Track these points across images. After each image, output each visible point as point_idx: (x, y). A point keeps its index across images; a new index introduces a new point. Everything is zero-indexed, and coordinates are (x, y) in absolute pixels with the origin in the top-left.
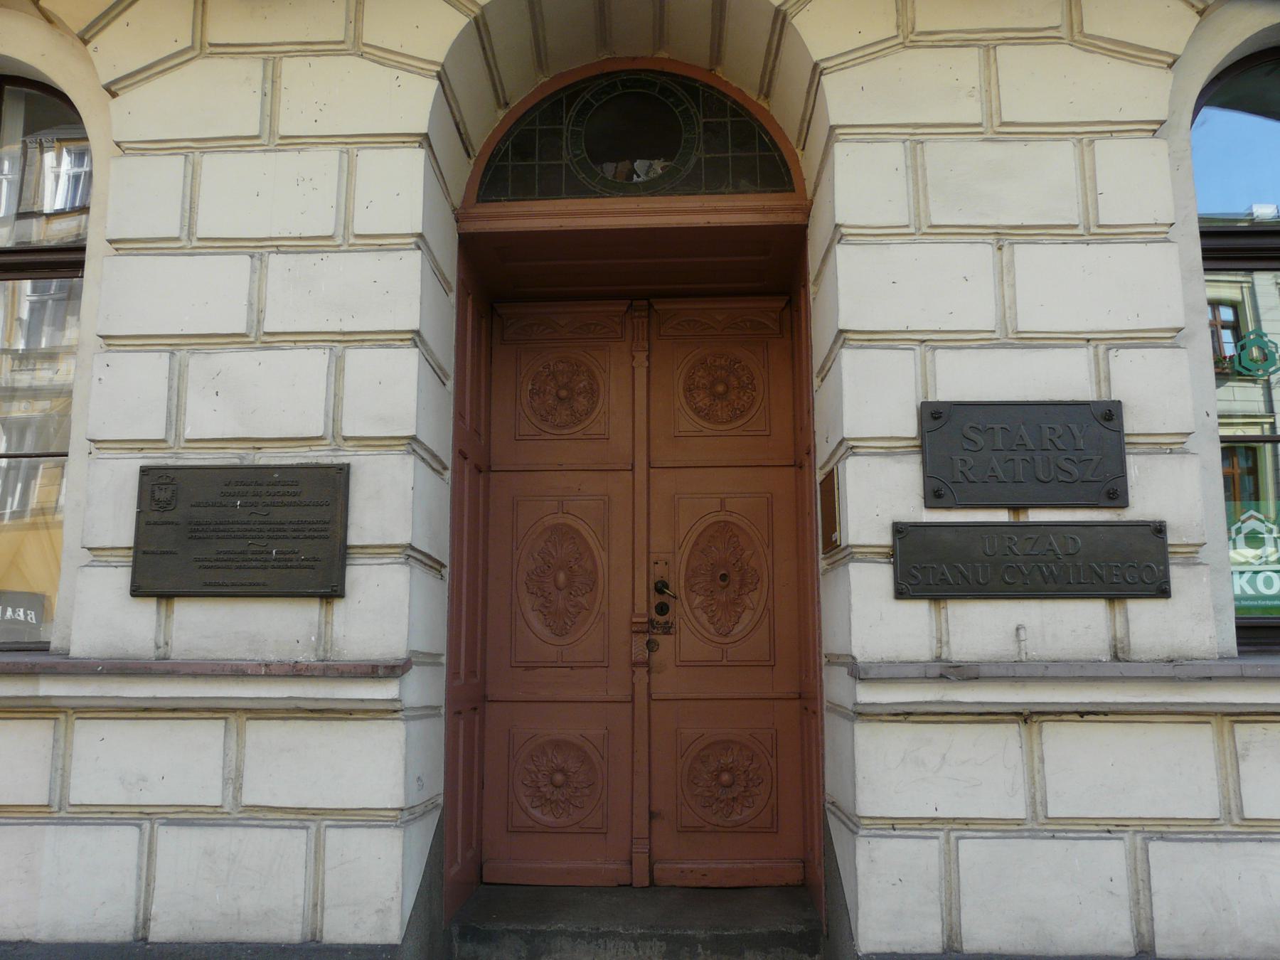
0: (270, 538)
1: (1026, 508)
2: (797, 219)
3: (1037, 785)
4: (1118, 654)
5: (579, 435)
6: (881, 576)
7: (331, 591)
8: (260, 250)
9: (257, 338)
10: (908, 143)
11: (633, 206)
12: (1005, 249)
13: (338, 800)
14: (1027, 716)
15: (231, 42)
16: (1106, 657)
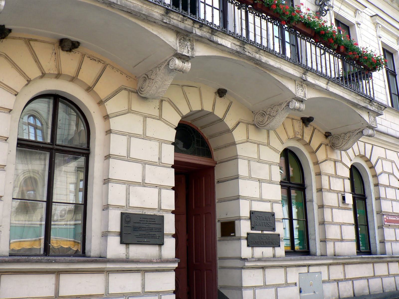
0: (150, 231)
1: (263, 231)
4: (274, 256)
14: (263, 268)
15: (382, 166)
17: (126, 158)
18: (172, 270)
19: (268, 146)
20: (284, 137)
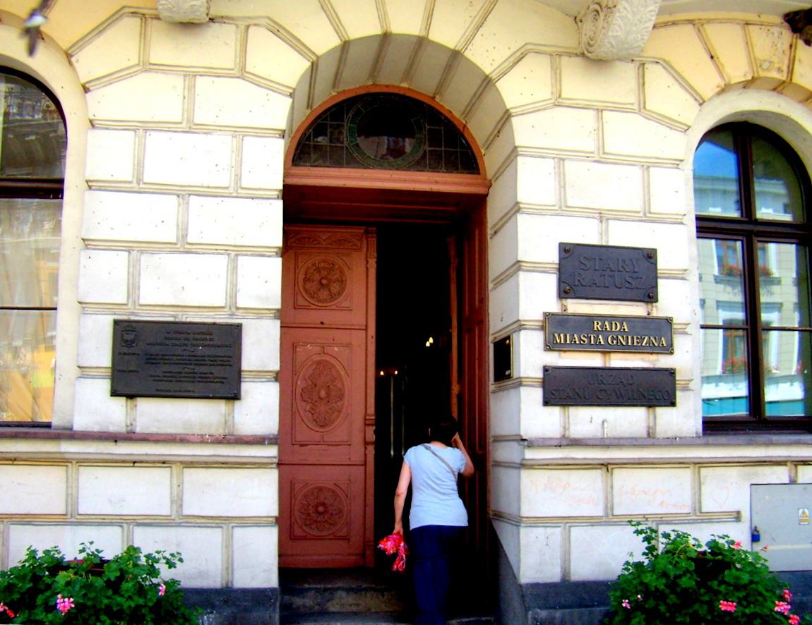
0: (196, 364)
2: (481, 190)
3: (609, 500)
5: (334, 307)
6: (538, 393)
7: (235, 396)
8: (182, 192)
9: (183, 246)
10: (556, 159)
11: (388, 176)
12: (604, 222)
13: (219, 511)
16: (645, 435)
17: (134, 185)
18: (272, 464)
19: (639, 112)
20: (707, 82)
